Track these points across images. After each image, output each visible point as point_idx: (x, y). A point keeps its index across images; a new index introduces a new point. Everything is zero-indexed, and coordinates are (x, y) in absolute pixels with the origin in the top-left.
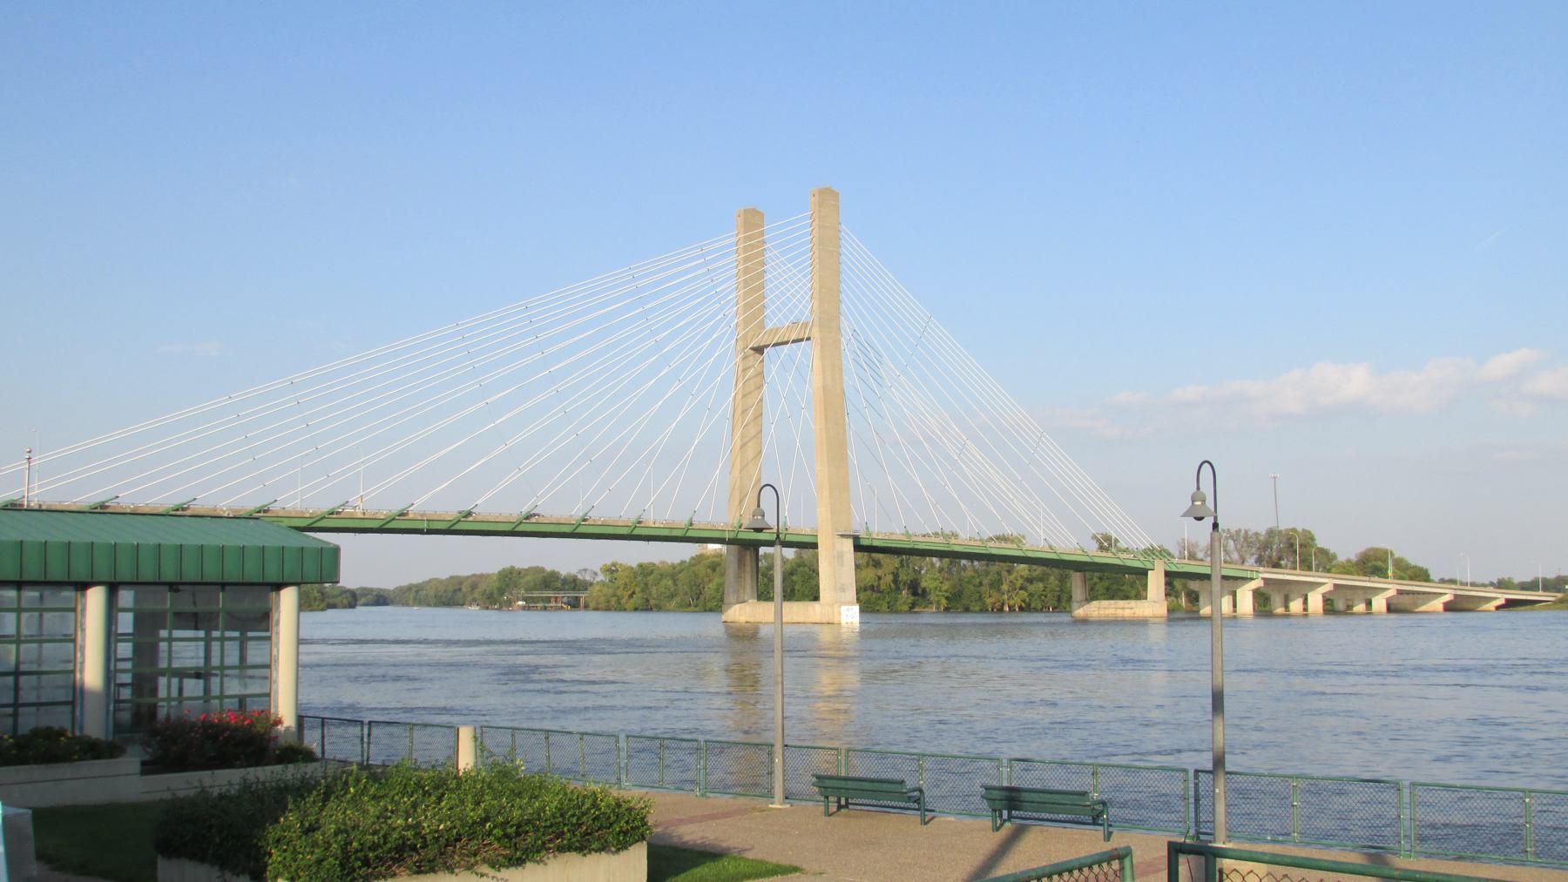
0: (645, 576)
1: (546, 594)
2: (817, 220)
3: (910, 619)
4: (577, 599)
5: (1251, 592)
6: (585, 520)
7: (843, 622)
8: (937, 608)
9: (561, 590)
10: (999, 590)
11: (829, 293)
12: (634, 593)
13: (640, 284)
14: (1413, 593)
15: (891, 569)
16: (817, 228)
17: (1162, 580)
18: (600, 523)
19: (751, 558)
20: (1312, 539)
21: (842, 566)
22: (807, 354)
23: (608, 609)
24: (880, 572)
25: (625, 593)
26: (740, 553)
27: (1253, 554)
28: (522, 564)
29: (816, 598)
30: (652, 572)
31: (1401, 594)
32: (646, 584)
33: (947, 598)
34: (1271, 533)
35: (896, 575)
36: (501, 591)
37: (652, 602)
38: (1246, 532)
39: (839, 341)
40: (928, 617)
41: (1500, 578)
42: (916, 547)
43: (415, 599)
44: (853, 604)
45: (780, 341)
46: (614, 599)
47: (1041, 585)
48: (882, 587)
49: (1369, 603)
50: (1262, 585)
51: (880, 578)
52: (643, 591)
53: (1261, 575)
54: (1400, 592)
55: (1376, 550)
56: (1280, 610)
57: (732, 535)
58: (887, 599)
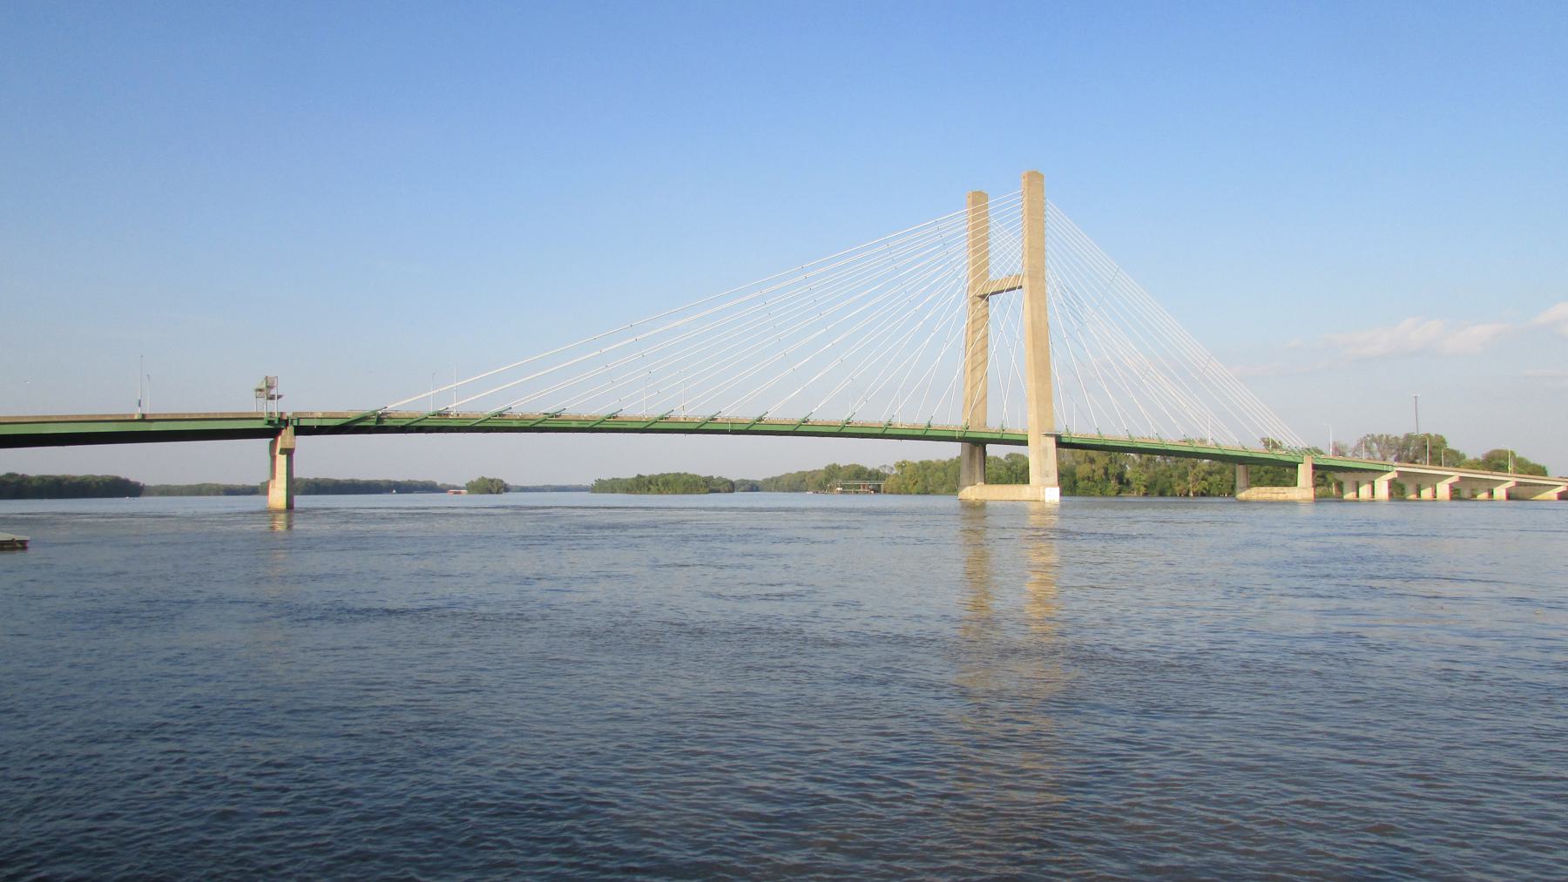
0: (925, 470)
5: (1387, 482)
6: (805, 422)
7: (1047, 500)
8: (1138, 493)
10: (1185, 480)
11: (1036, 253)
14: (1531, 484)
17: (1310, 471)
20: (1444, 442)
22: (1021, 299)
24: (1094, 467)
26: (971, 448)
27: (1394, 454)
28: (843, 462)
29: (1026, 481)
30: (929, 467)
31: (1521, 485)
32: (926, 476)
33: (1145, 486)
34: (1408, 437)
35: (1106, 470)
36: (827, 481)
37: (930, 488)
38: (1387, 437)
39: (1044, 288)
40: (1132, 498)
43: (775, 487)
44: (1052, 486)
47: (1218, 477)
48: (1096, 478)
49: (1491, 494)
50: (1396, 476)
51: (1094, 471)
52: (923, 480)
53: (1396, 469)
54: (1518, 484)
55: (1499, 452)
56: (1413, 497)
57: (961, 435)
58: (1100, 487)
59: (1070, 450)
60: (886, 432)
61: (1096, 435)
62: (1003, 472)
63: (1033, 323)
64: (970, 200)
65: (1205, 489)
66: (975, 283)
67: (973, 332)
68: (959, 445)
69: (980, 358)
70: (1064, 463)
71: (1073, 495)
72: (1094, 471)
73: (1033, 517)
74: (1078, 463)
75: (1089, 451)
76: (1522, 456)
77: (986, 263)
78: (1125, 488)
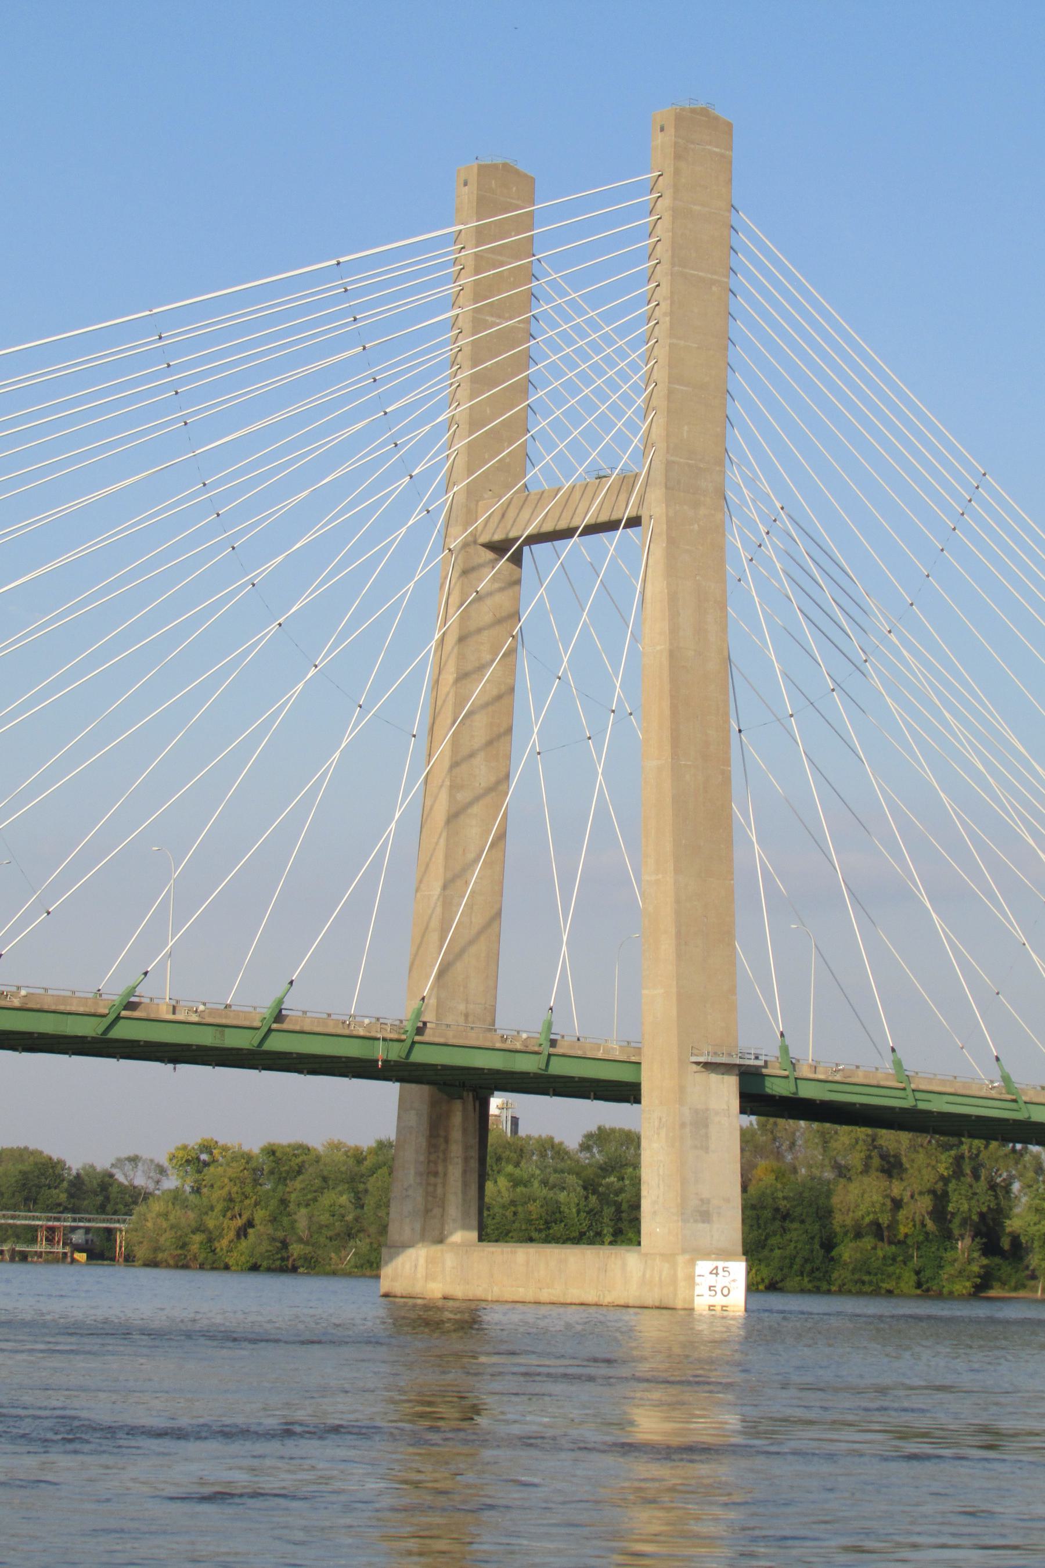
0: (282, 1180)
1: (23, 1220)
2: (668, 194)
3: (980, 1310)
4: (109, 1234)
9: (66, 1210)
12: (250, 1224)
13: (148, 343)
15: (929, 1178)
16: (667, 217)
18: (16, 1003)
19: (465, 1118)
21: (706, 1149)
23: (182, 1264)
24: (897, 1189)
25: (226, 1222)
26: (434, 1104)
32: (284, 1202)
35: (940, 1199)
37: (296, 1249)
39: (720, 530)
42: (922, 1106)
44: (724, 1255)
45: (548, 527)
46: (198, 1238)
51: (897, 1204)
52: (274, 1220)
57: (395, 1053)
59: (815, 1125)
60: (114, 1034)
62: (569, 1199)
63: (674, 655)
64: (467, 195)
66: (473, 493)
67: (463, 677)
68: (390, 1091)
69: (482, 773)
70: (795, 1170)
71: (817, 1291)
72: (897, 1204)
73: (446, 1313)
74: (842, 1171)
75: (883, 1132)
77: (520, 425)
78: (1006, 1269)
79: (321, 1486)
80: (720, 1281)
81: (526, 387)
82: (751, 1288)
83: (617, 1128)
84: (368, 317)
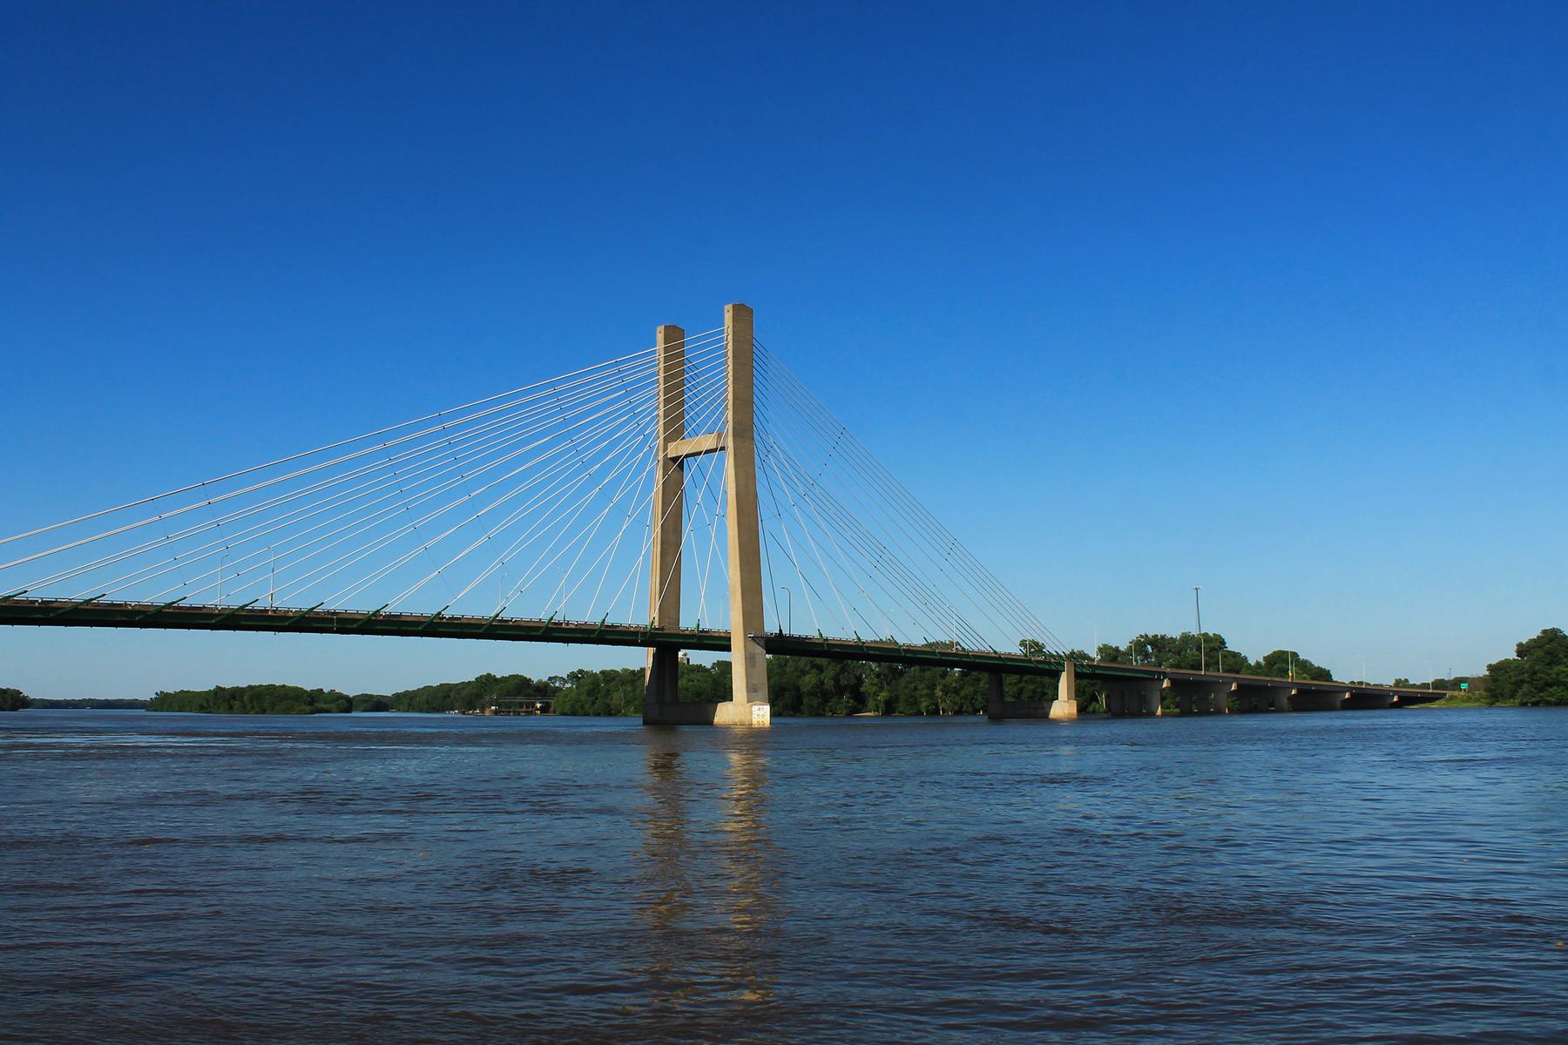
13: (550, 391)
15: (832, 673)
20: (1223, 642)
21: (754, 666)
30: (614, 679)
37: (613, 712)
41: (1398, 678)
61: (817, 635)
65: (678, 766)
76: (1306, 658)
77: (681, 416)
79: (250, 988)
80: (761, 712)
81: (682, 403)
82: (772, 715)
83: (1261, 660)
84: (628, 380)
